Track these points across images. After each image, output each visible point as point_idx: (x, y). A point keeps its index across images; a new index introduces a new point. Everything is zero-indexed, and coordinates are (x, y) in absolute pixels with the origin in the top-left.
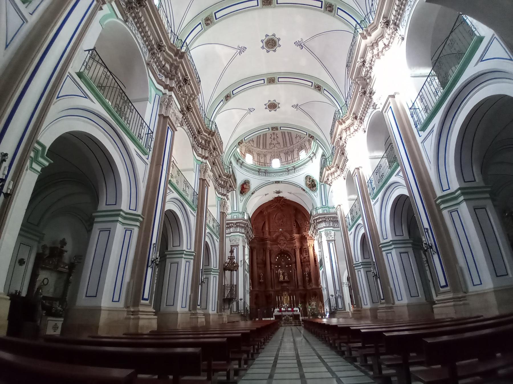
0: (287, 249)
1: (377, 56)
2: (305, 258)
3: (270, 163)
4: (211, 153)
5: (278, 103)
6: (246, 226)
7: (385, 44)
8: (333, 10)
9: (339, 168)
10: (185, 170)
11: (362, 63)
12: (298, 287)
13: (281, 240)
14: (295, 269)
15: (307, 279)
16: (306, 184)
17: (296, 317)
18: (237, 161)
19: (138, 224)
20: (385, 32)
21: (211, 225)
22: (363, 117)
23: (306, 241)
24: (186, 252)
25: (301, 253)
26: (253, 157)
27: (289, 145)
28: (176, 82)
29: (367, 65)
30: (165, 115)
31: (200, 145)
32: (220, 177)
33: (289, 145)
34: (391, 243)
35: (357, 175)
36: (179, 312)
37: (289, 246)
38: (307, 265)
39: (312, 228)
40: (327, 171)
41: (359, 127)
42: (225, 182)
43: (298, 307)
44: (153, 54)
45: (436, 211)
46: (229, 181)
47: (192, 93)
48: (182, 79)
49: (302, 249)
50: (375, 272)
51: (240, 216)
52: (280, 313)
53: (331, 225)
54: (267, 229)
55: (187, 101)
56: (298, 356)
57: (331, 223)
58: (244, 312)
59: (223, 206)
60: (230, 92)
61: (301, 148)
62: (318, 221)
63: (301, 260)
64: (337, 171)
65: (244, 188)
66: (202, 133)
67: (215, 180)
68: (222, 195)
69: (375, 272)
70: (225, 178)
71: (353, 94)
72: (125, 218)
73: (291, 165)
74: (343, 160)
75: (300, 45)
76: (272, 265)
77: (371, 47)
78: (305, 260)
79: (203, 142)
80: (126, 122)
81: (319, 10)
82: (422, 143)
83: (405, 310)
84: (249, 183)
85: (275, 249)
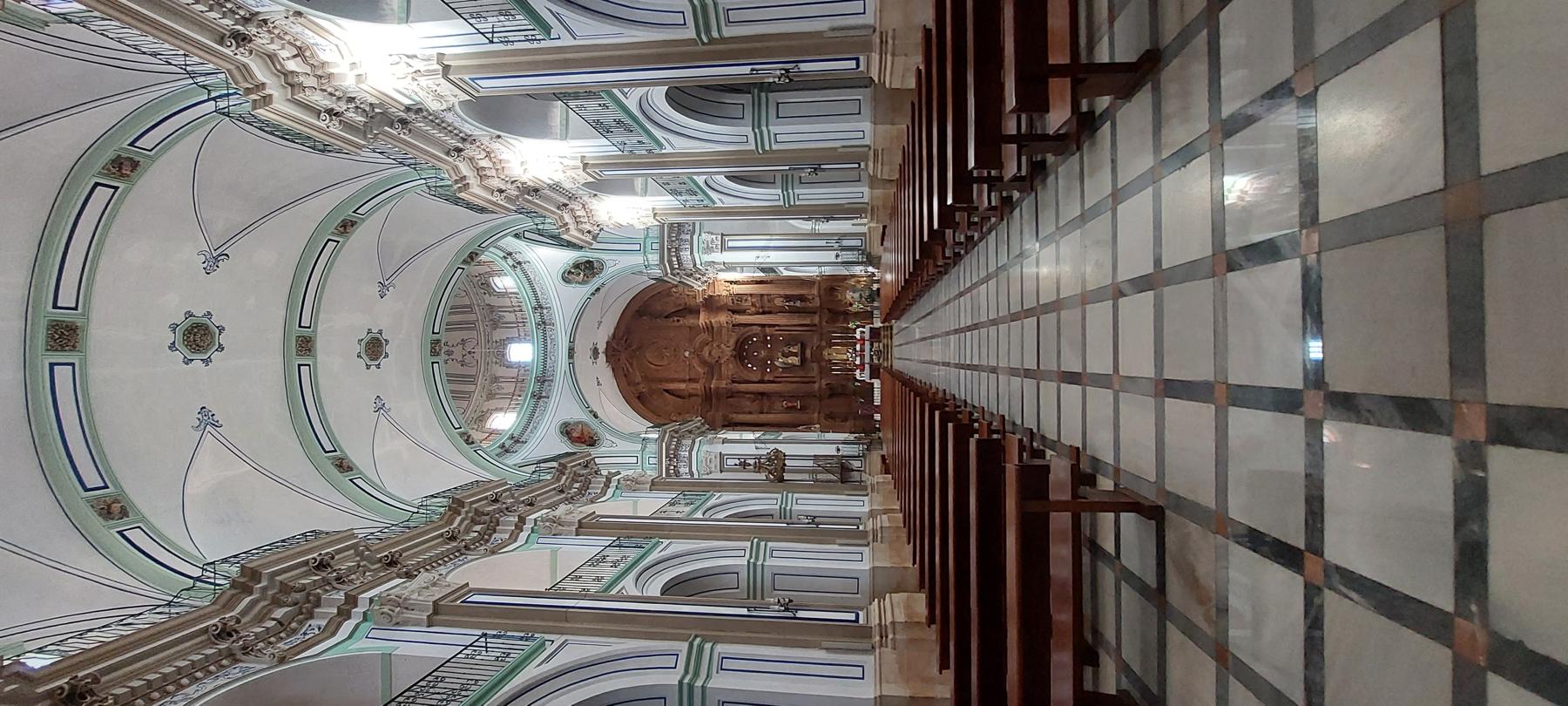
0: (732, 342)
1: (323, 82)
2: (753, 305)
3: (519, 366)
4: (507, 509)
5: (368, 333)
6: (676, 435)
7: (295, 56)
8: (132, 159)
9: (568, 205)
10: (554, 572)
11: (334, 117)
12: (815, 325)
13: (710, 353)
14: (777, 328)
15: (798, 304)
16: (583, 282)
17: (875, 334)
18: (507, 451)
19: (708, 646)
20: (261, 47)
21: (688, 509)
22: (461, 135)
23: (717, 298)
24: (751, 557)
25: (743, 312)
26: (498, 410)
27: (472, 317)
28: (327, 591)
29: (341, 107)
30: (431, 611)
31: (486, 537)
32: (562, 491)
33: (472, 317)
34: (757, 130)
35: (472, 79)
36: (871, 566)
37: (725, 338)
38: (769, 301)
39: (690, 281)
40: (275, 105)
41: (482, 147)
42: (478, 519)
43: (856, 329)
44: (246, 650)
45: (721, 47)
46: (574, 469)
47: (352, 551)
48: (316, 575)
49: (735, 308)
50: (809, 170)
51: (652, 448)
52: (867, 366)
53: (688, 237)
54: (683, 386)
55: (373, 564)
56: (956, 331)
57: (684, 237)
58: (863, 444)
59: (637, 483)
60: (329, 458)
61: (486, 287)
62: (677, 266)
63: (758, 313)
64: (572, 210)
65: (578, 435)
66: (456, 530)
67: (570, 503)
68: (607, 486)
69: (809, 170)
70: (564, 477)
71: (397, 149)
72: (696, 674)
73: (530, 316)
74: (549, 193)
75: (214, 260)
76: (766, 378)
77: (296, 91)
78: (758, 305)
79: (478, 530)
80: (473, 688)
81: (121, 200)
82: (575, 39)
83: (881, 128)
84: (570, 424)
85: (729, 369)
